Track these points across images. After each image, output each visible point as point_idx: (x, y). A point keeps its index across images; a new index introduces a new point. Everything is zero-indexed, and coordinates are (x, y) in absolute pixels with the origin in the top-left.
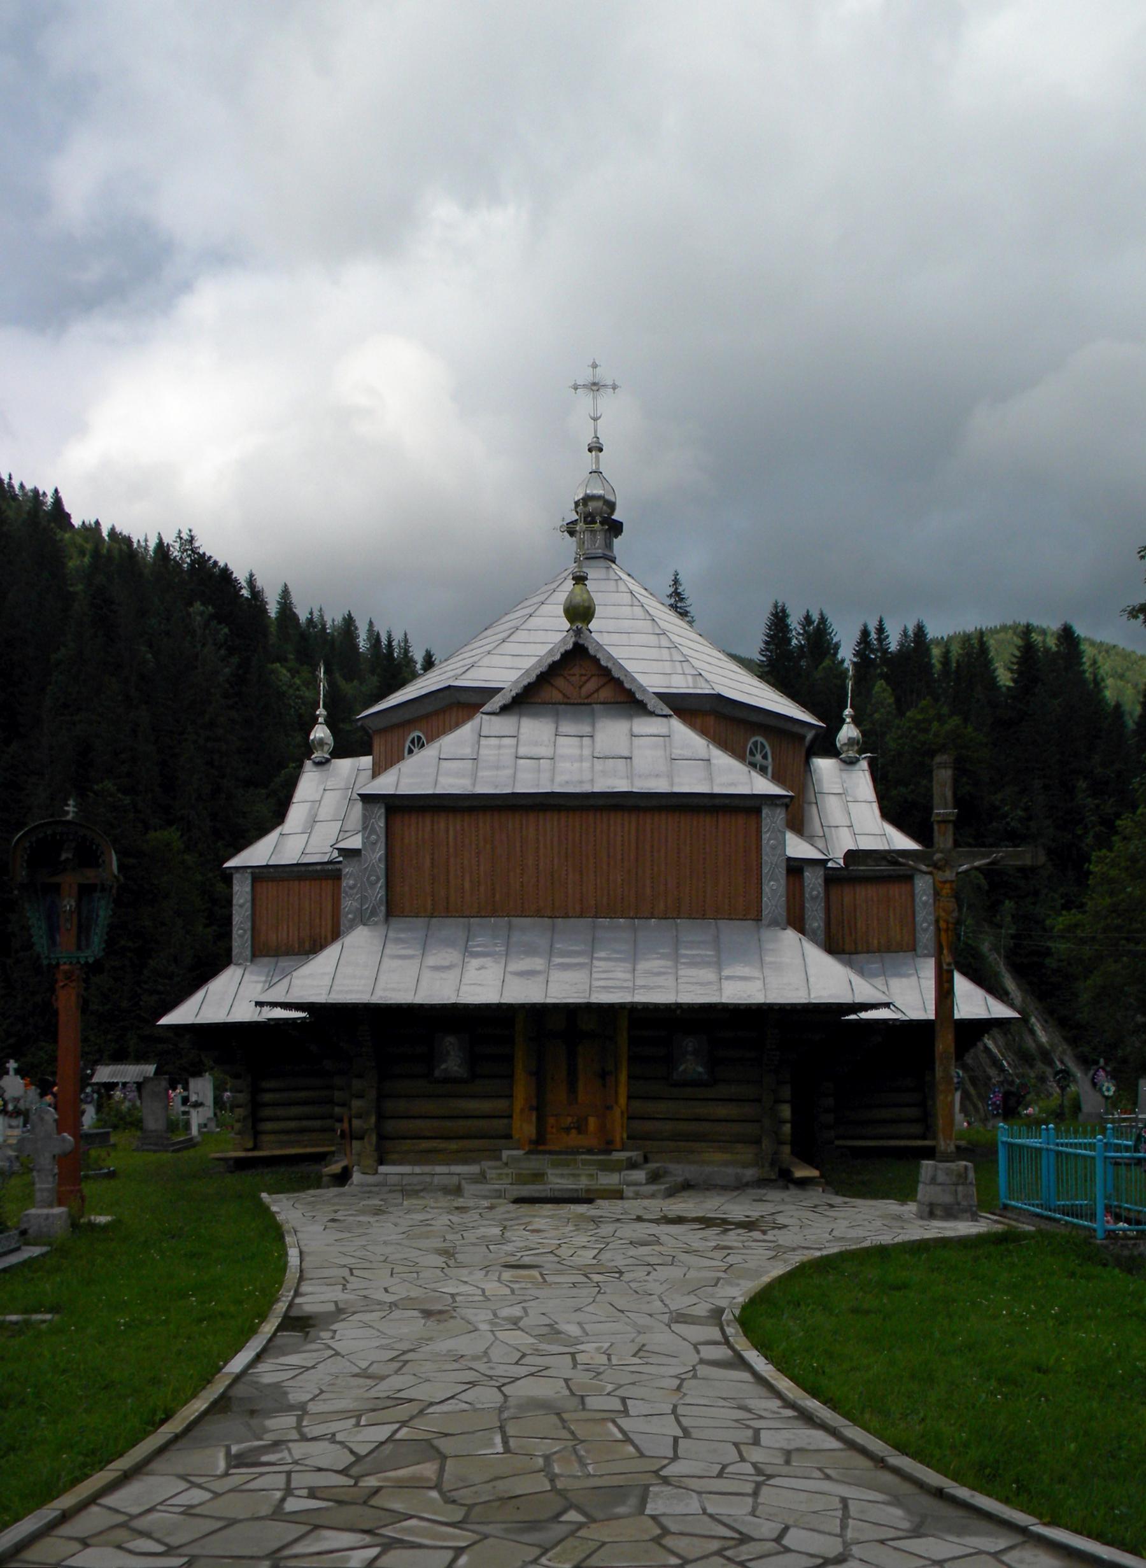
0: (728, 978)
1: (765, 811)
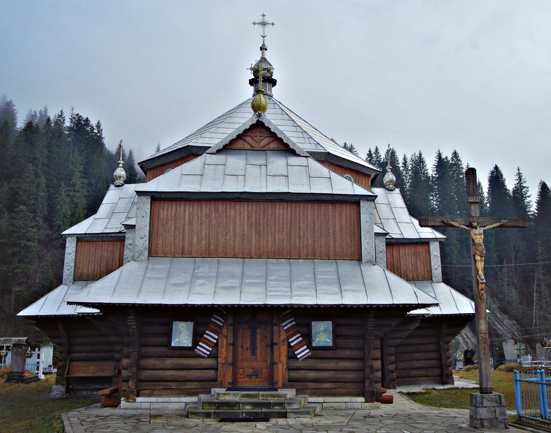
0: (346, 290)
1: (362, 204)
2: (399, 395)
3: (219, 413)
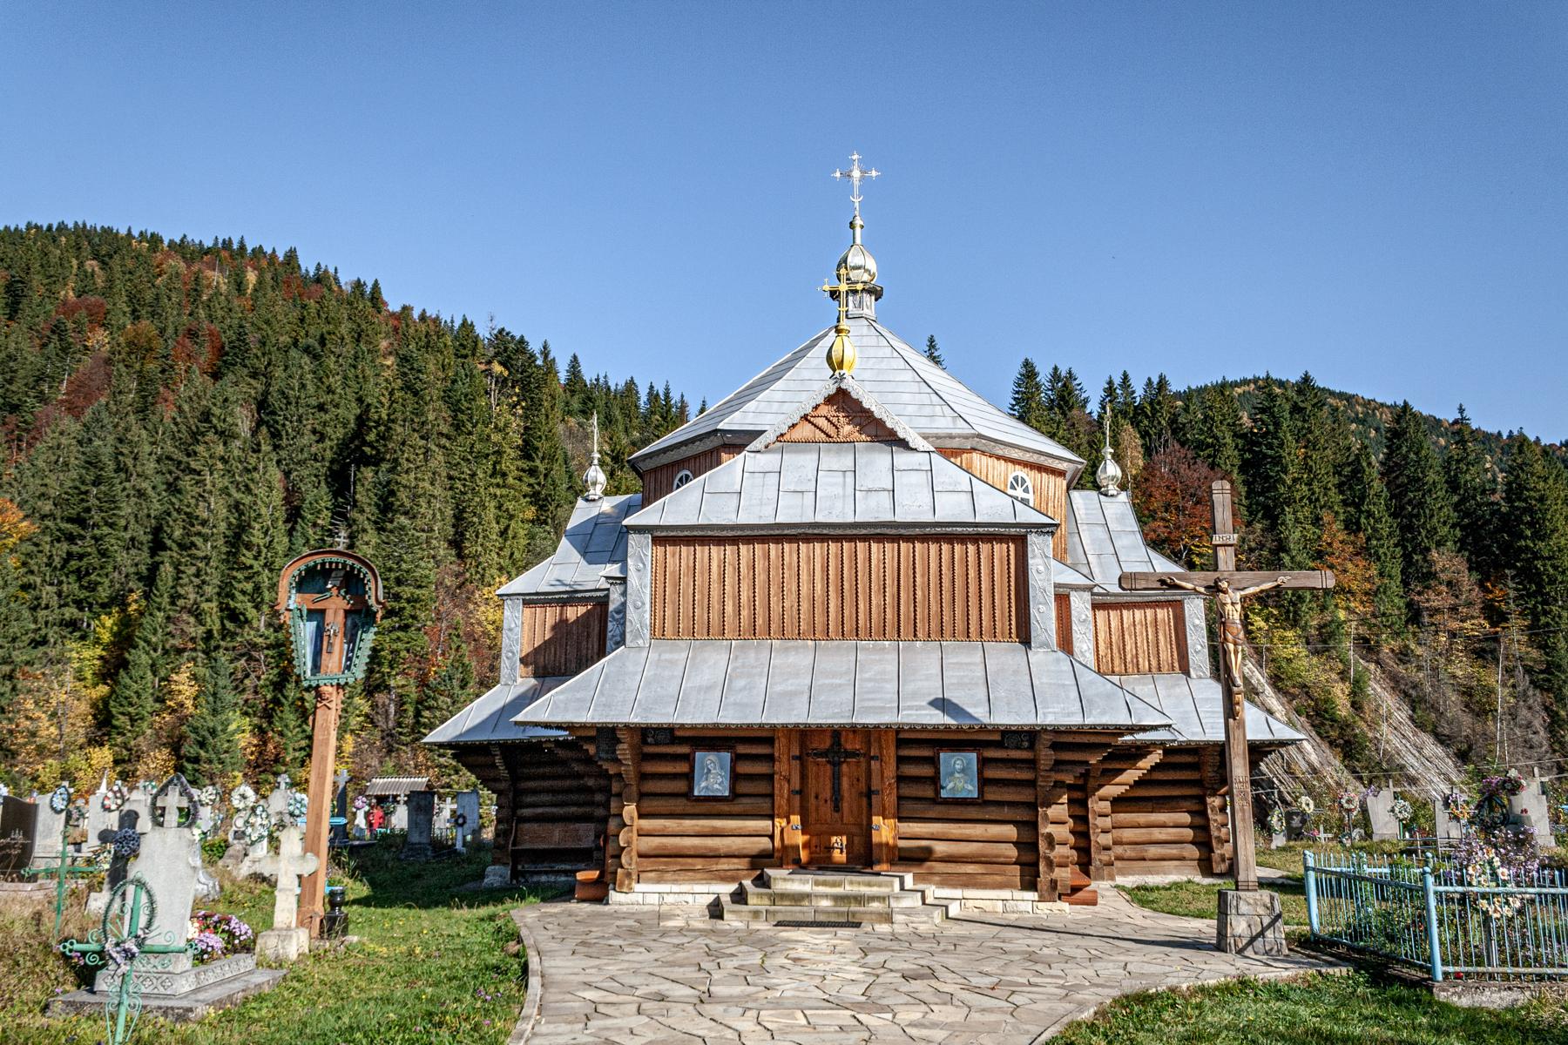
1: (1032, 539)
2: (1114, 892)
3: (774, 913)
